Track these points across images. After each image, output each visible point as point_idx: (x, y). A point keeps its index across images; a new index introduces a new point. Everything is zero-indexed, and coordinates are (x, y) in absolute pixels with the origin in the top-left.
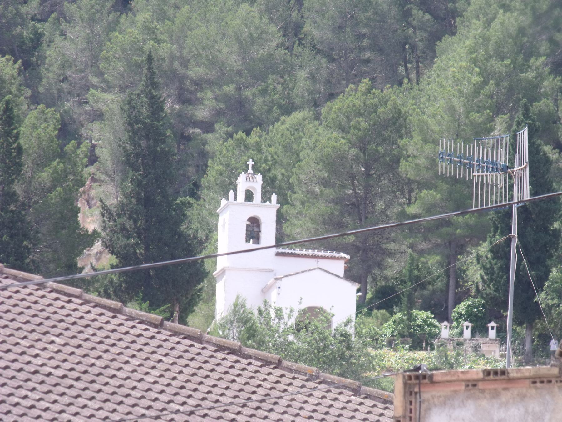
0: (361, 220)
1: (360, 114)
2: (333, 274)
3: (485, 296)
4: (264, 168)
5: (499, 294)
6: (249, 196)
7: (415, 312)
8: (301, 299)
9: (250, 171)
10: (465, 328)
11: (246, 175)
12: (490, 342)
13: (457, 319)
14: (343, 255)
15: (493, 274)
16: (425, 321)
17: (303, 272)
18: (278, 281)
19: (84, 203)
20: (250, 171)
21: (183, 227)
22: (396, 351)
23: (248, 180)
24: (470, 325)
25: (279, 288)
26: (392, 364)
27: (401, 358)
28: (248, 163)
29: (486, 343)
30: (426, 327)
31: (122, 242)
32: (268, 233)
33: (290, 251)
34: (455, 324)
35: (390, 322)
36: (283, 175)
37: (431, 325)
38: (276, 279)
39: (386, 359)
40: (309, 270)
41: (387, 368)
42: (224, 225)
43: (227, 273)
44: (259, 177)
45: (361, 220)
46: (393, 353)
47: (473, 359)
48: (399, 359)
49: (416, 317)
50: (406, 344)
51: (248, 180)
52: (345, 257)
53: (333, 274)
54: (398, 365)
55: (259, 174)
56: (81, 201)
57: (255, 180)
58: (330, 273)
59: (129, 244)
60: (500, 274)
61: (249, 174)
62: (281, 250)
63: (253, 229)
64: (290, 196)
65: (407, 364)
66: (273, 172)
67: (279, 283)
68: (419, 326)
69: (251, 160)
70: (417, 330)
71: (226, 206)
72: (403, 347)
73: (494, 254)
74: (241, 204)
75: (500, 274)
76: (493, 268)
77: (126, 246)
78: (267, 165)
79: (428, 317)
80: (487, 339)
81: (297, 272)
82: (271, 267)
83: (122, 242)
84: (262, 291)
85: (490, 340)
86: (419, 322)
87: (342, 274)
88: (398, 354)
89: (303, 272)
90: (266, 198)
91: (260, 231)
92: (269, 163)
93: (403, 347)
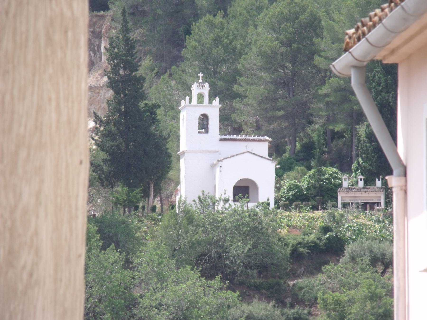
0: (289, 94)
1: (287, 20)
2: (258, 155)
3: (363, 169)
4: (226, 42)
5: (373, 168)
6: (201, 97)
7: (324, 169)
8: (225, 191)
9: (201, 81)
10: (359, 180)
11: (198, 84)
12: (378, 190)
13: (356, 171)
14: (267, 138)
15: (368, 154)
16: (331, 175)
17: (237, 155)
18: (220, 162)
19: (107, 40)
20: (201, 81)
21: (153, 128)
22: (300, 212)
23: (199, 88)
24: (363, 177)
25: (221, 167)
26: (297, 222)
27: (304, 218)
28: (199, 75)
29: (374, 191)
30: (332, 180)
31: (109, 144)
32: (214, 123)
33: (230, 137)
34: (354, 175)
35: (307, 176)
36: (241, 45)
37: (336, 178)
38: (218, 161)
39: (293, 219)
40: (241, 154)
41: (293, 226)
42: (183, 119)
43: (186, 154)
44: (207, 85)
45: (289, 94)
46: (298, 214)
47: (355, 214)
48: (302, 219)
49: (325, 172)
50: (308, 207)
51: (199, 88)
52: (268, 140)
53: (258, 155)
54: (301, 223)
55: (207, 83)
56: (104, 38)
57: (204, 88)
58: (256, 155)
59: (114, 145)
60: (373, 154)
61: (200, 83)
62: (223, 137)
63: (204, 123)
64: (239, 79)
65: (307, 223)
66: (233, 44)
67: (220, 164)
68: (327, 179)
69: (201, 73)
70: (325, 182)
71: (184, 107)
72: (306, 209)
73: (369, 140)
74: (194, 106)
75: (373, 154)
76: (368, 150)
77: (112, 146)
78: (228, 39)
79: (333, 173)
80: (375, 187)
81: (232, 155)
82: (216, 149)
83: (109, 144)
84: (211, 166)
85: (377, 188)
86: (327, 176)
87: (266, 155)
88: (302, 215)
89: (237, 155)
90: (212, 98)
91: (208, 124)
92: (231, 38)
93: (306, 209)
